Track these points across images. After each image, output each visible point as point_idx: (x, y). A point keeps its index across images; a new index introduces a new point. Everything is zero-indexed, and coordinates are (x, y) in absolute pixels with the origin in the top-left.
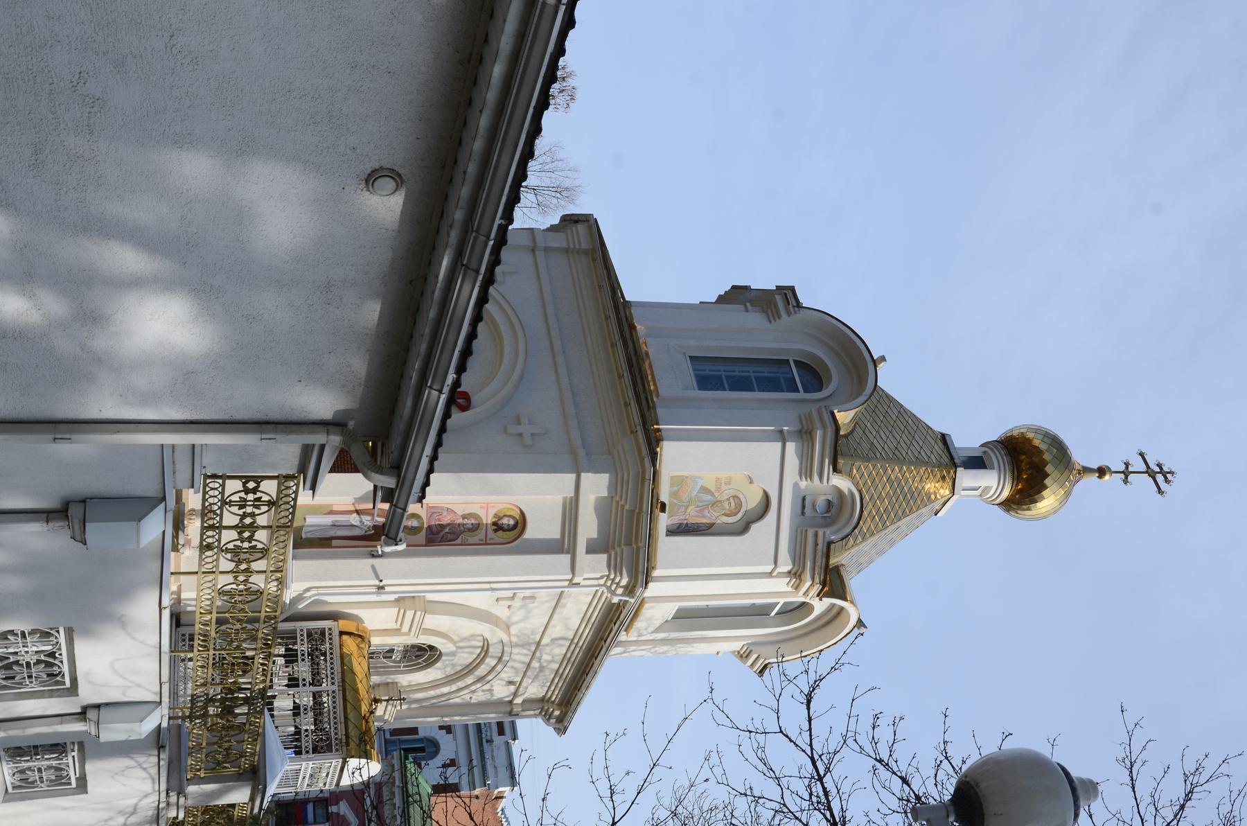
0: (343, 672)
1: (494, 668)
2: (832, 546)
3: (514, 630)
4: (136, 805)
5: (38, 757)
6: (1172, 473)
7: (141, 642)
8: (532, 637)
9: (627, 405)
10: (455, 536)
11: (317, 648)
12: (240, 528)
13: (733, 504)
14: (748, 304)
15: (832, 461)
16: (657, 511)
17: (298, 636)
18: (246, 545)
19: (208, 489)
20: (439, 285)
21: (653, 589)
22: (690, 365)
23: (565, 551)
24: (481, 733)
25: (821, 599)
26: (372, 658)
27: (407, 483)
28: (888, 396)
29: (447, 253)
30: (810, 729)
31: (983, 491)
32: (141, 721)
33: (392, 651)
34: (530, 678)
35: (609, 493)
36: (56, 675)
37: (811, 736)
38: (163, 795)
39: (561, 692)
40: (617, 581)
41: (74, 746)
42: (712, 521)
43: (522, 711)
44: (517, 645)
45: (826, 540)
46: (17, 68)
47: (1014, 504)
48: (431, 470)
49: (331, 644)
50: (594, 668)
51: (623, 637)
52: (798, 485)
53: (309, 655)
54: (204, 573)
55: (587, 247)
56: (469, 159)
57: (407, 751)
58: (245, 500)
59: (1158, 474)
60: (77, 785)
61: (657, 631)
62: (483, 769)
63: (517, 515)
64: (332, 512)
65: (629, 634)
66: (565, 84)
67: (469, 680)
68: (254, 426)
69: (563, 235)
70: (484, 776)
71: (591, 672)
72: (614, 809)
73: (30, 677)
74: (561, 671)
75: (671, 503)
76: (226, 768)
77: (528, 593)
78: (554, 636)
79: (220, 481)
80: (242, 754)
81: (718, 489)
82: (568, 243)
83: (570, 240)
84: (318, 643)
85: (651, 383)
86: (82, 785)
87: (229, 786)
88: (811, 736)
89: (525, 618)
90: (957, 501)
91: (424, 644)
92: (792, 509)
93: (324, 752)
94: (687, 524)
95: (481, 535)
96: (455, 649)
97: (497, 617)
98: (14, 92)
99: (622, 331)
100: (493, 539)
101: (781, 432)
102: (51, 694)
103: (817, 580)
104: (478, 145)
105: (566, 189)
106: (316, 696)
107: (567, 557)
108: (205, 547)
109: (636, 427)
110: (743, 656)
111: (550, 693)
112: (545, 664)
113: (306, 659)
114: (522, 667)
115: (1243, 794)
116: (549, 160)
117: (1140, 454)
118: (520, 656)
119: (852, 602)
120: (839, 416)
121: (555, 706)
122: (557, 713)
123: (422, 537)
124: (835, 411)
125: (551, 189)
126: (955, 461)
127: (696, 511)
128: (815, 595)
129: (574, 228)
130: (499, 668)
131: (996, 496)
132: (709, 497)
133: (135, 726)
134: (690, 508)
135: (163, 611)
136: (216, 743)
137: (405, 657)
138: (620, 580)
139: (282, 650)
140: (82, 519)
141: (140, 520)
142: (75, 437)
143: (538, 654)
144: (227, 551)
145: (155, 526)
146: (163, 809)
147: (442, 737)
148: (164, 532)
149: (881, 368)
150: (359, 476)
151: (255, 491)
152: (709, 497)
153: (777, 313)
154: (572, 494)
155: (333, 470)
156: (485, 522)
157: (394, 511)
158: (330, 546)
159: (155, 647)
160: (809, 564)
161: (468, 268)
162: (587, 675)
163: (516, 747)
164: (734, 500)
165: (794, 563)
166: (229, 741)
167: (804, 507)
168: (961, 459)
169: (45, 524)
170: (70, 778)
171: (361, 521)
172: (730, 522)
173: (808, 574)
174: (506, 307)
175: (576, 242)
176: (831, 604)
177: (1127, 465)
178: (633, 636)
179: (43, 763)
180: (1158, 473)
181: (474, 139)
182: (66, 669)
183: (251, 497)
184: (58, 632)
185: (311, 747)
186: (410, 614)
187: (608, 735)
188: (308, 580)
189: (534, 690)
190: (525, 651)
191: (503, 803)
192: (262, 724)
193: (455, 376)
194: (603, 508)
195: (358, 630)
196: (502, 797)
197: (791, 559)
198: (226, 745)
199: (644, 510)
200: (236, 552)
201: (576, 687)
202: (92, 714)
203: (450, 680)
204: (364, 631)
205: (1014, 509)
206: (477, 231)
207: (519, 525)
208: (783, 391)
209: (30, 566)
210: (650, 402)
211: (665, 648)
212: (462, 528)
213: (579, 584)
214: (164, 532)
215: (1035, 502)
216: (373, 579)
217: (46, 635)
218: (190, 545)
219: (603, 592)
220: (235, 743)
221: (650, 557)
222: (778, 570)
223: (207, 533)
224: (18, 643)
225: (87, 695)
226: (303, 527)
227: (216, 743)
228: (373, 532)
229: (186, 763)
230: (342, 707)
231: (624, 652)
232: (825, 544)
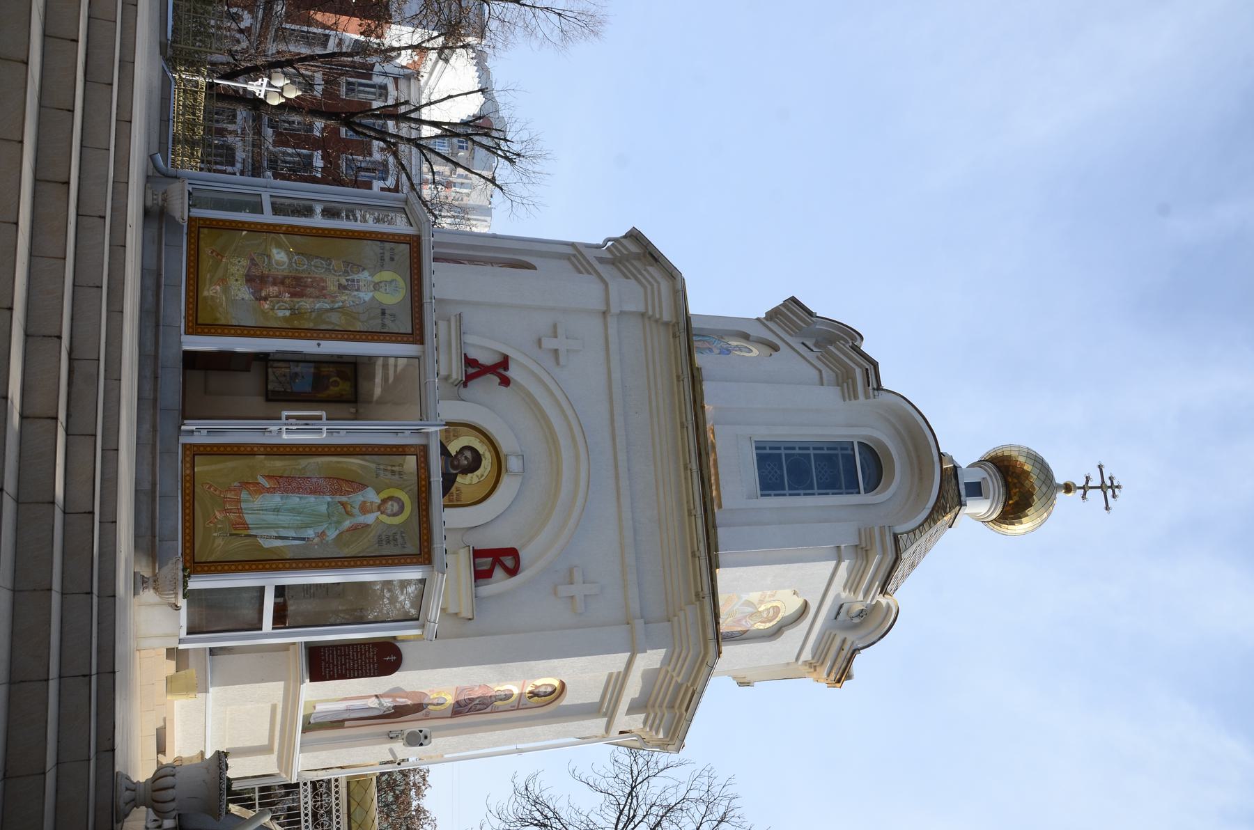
11: (322, 804)
42: (747, 629)
84: (320, 803)
85: (714, 488)
100: (526, 704)
126: (962, 499)
153: (854, 391)
158: (343, 727)
165: (813, 658)
167: (838, 613)
174: (569, 412)
177: (1088, 479)
232: (851, 651)
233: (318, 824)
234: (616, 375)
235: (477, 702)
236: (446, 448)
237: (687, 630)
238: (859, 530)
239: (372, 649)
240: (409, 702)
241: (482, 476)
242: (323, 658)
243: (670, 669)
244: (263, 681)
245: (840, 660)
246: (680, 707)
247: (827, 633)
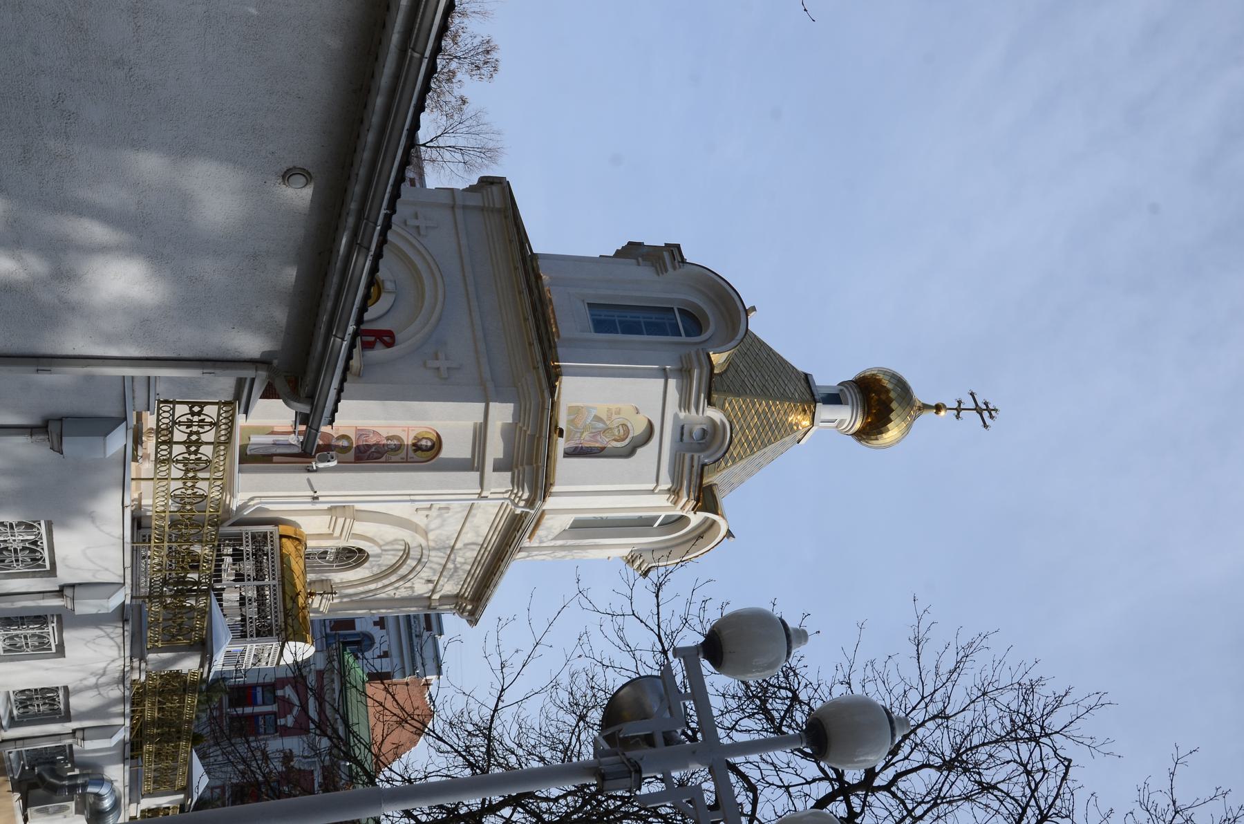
0: (282, 569)
1: (414, 568)
2: (706, 468)
3: (431, 536)
4: (105, 668)
5: (24, 627)
6: (995, 410)
7: (108, 534)
8: (447, 542)
9: (531, 344)
10: (379, 455)
12: (199, 443)
13: (622, 431)
14: (640, 259)
16: (555, 436)
17: (244, 538)
18: (193, 457)
19: (161, 412)
20: (340, 258)
21: (551, 503)
22: (588, 312)
24: (411, 629)
25: (695, 513)
26: (309, 558)
27: (319, 410)
28: (759, 340)
29: (346, 234)
30: (658, 614)
32: (109, 598)
33: (326, 552)
34: (446, 577)
35: (514, 418)
36: (39, 560)
37: (658, 618)
38: (128, 660)
39: (473, 590)
40: (519, 495)
41: (53, 618)
42: (604, 446)
43: (439, 605)
44: (434, 549)
45: (700, 463)
46: (11, 89)
47: (864, 434)
48: (338, 400)
49: (272, 545)
51: (526, 543)
52: (678, 415)
53: (253, 554)
54: (158, 479)
56: (360, 165)
57: (346, 644)
58: (192, 421)
59: (984, 411)
60: (56, 650)
61: (555, 539)
62: (413, 661)
63: (434, 438)
64: (273, 433)
65: (532, 542)
66: (489, 57)
67: (393, 578)
68: (198, 362)
69: (479, 195)
70: (413, 666)
71: (498, 572)
72: (504, 679)
73: (17, 561)
74: (473, 571)
75: (569, 430)
76: (180, 640)
77: (443, 504)
78: (466, 542)
79: (171, 406)
80: (193, 629)
81: (609, 418)
82: (484, 204)
83: (486, 200)
85: (553, 326)
86: (61, 651)
87: (181, 655)
88: (658, 618)
90: (816, 431)
92: (672, 434)
93: (266, 636)
95: (403, 454)
97: (417, 525)
98: (8, 107)
99: (528, 281)
100: (413, 458)
101: (665, 369)
102: (34, 575)
103: (692, 497)
104: (366, 155)
105: (490, 150)
106: (260, 589)
107: (477, 474)
108: (158, 461)
109: (538, 363)
110: (631, 560)
111: (467, 594)
112: (458, 566)
113: (251, 558)
114: (439, 568)
115: (1002, 663)
116: (475, 123)
117: (971, 394)
118: (437, 558)
119: (723, 517)
120: (714, 357)
122: (469, 607)
124: (711, 353)
125: (475, 149)
126: (815, 397)
127: (589, 436)
129: (489, 190)
130: (419, 568)
132: (601, 425)
133: (103, 602)
134: (585, 434)
135: (126, 509)
136: (171, 619)
137: (337, 558)
138: (522, 495)
139: (230, 551)
140: (59, 434)
141: (106, 435)
142: (54, 369)
143: (452, 557)
144: (178, 462)
145: (118, 441)
146: (128, 672)
147: (377, 632)
148: (125, 445)
149: (752, 316)
150: (279, 403)
151: (199, 413)
152: (601, 425)
154: (481, 420)
155: (264, 396)
156: (406, 443)
157: (310, 431)
158: (271, 462)
159: (119, 538)
160: (685, 483)
161: (362, 246)
162: (495, 575)
163: (442, 641)
165: (673, 482)
166: (181, 618)
167: (682, 434)
168: (821, 396)
169: (29, 438)
170: (50, 645)
172: (619, 446)
173: (685, 492)
174: (428, 257)
176: (705, 517)
177: (960, 402)
178: (535, 543)
179: (28, 631)
180: (984, 410)
181: (363, 151)
182: (46, 554)
183: (196, 418)
184: (40, 524)
185: (255, 631)
186: (341, 521)
187: (500, 620)
190: (442, 554)
192: (208, 604)
193: (355, 327)
194: (509, 434)
195: (296, 534)
198: (179, 621)
199: (544, 434)
200: (185, 462)
201: (485, 586)
202: (68, 592)
203: (376, 578)
204: (301, 535)
205: (864, 439)
206: (367, 219)
207: (436, 447)
208: (667, 335)
209: (20, 470)
210: (552, 342)
211: (563, 553)
212: (386, 448)
213: (487, 497)
214: (125, 445)
215: (881, 433)
216: (309, 491)
217: (29, 527)
218: (149, 459)
219: (508, 505)
220: (186, 619)
221: (548, 473)
222: (659, 488)
223: (161, 447)
224: (7, 533)
225: (65, 575)
226: (248, 444)
227: (171, 619)
229: (147, 635)
230: (281, 599)
231: (528, 557)
232: (700, 466)
234: (463, 241)
235: (373, 450)
238: (681, 357)
243: (521, 424)
247: (678, 454)
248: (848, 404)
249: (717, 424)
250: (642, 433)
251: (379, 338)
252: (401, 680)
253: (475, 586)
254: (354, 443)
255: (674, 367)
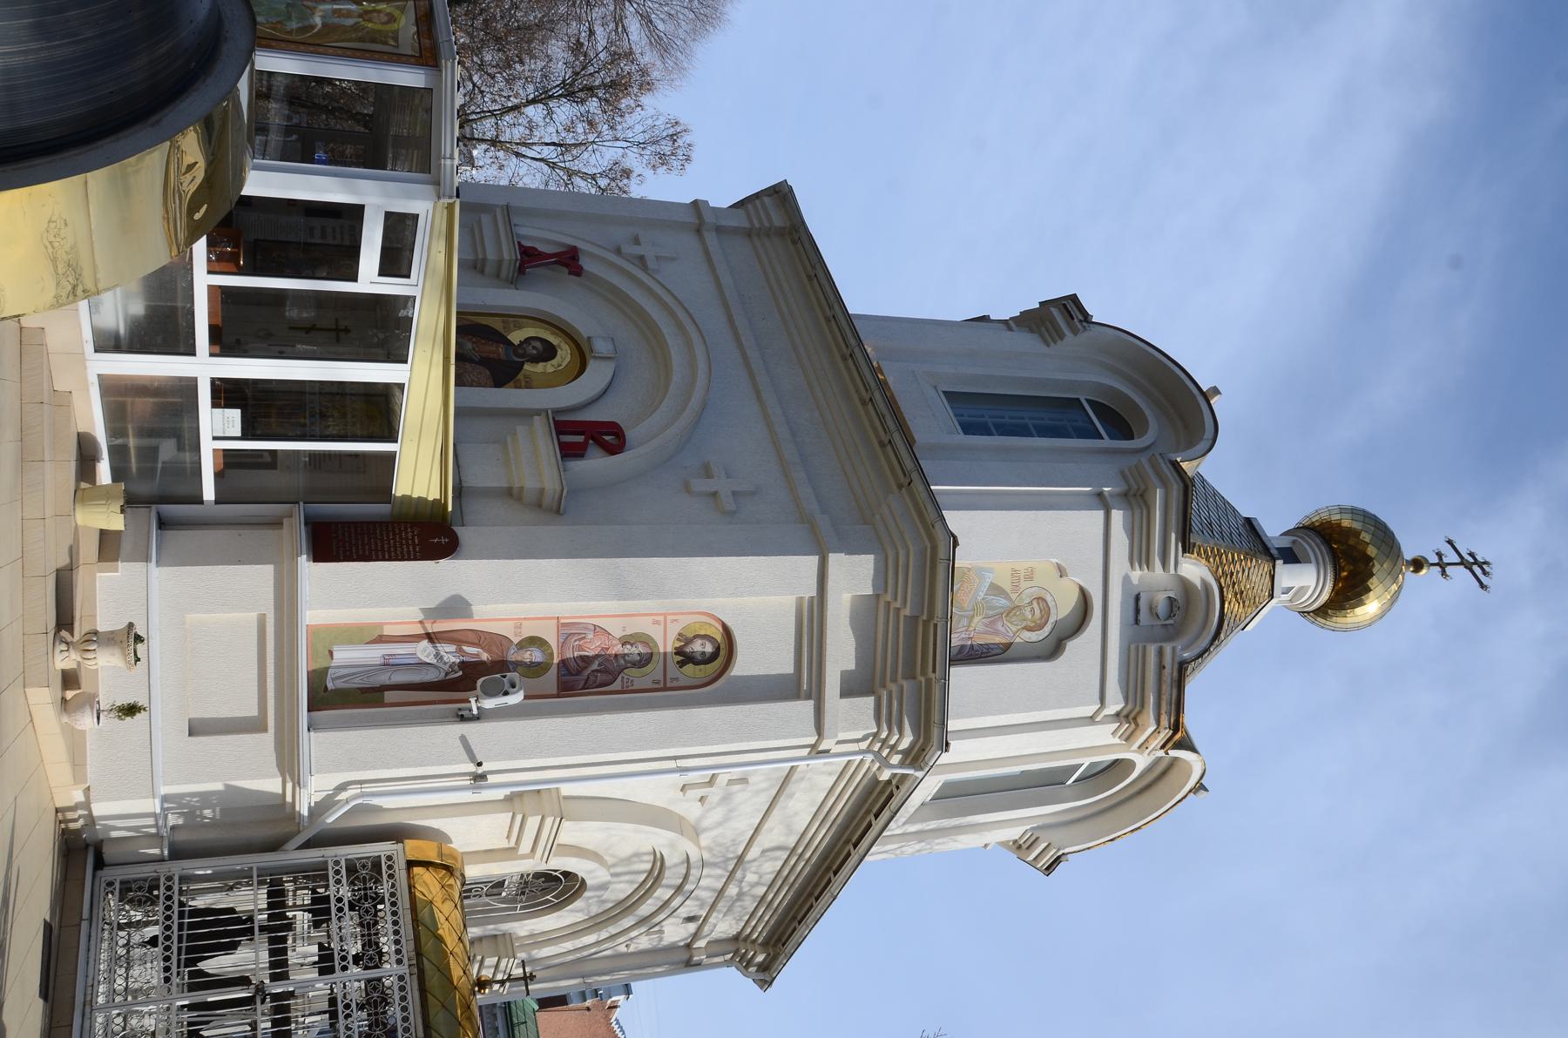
1: (666, 903)
6: (1485, 563)
15: (1180, 536)
17: (331, 873)
23: (803, 694)
26: (468, 897)
31: (1295, 594)
33: (500, 884)
45: (1177, 660)
50: (833, 888)
55: (782, 225)
59: (1474, 564)
64: (381, 639)
67: (628, 922)
77: (736, 772)
78: (767, 845)
81: (1016, 587)
84: (362, 892)
89: (726, 819)
91: (556, 871)
94: (972, 646)
95: (654, 671)
96: (608, 878)
97: (681, 818)
100: (677, 679)
101: (1100, 495)
103: (1165, 722)
107: (807, 706)
118: (711, 880)
121: (757, 948)
122: (760, 958)
123: (550, 680)
128: (1159, 746)
131: (1314, 598)
134: (976, 619)
139: (305, 897)
143: (739, 874)
152: (1003, 601)
153: (1056, 331)
154: (812, 592)
156: (662, 650)
158: (381, 704)
160: (1151, 700)
164: (1039, 604)
165: (1126, 700)
167: (1137, 611)
171: (437, 655)
172: (1034, 639)
175: (763, 217)
186: (534, 823)
188: (339, 768)
189: (723, 926)
191: (617, 1014)
194: (866, 615)
196: (616, 1007)
197: (1122, 693)
203: (596, 922)
212: (622, 662)
213: (827, 751)
226: (326, 670)
228: (461, 673)
230: (418, 1009)
232: (1176, 666)
233: (357, 878)
234: (726, 280)
235: (595, 666)
236: (506, 338)
237: (897, 526)
239: (411, 528)
240: (485, 656)
241: (560, 365)
242: (334, 535)
243: (889, 598)
244: (240, 562)
245: (1166, 688)
246: (924, 673)
247: (1133, 647)
248: (1311, 562)
249: (1197, 587)
250: (1069, 615)
251: (593, 438)
252: (580, 1005)
253: (772, 922)
254: (555, 655)
255: (1118, 490)
